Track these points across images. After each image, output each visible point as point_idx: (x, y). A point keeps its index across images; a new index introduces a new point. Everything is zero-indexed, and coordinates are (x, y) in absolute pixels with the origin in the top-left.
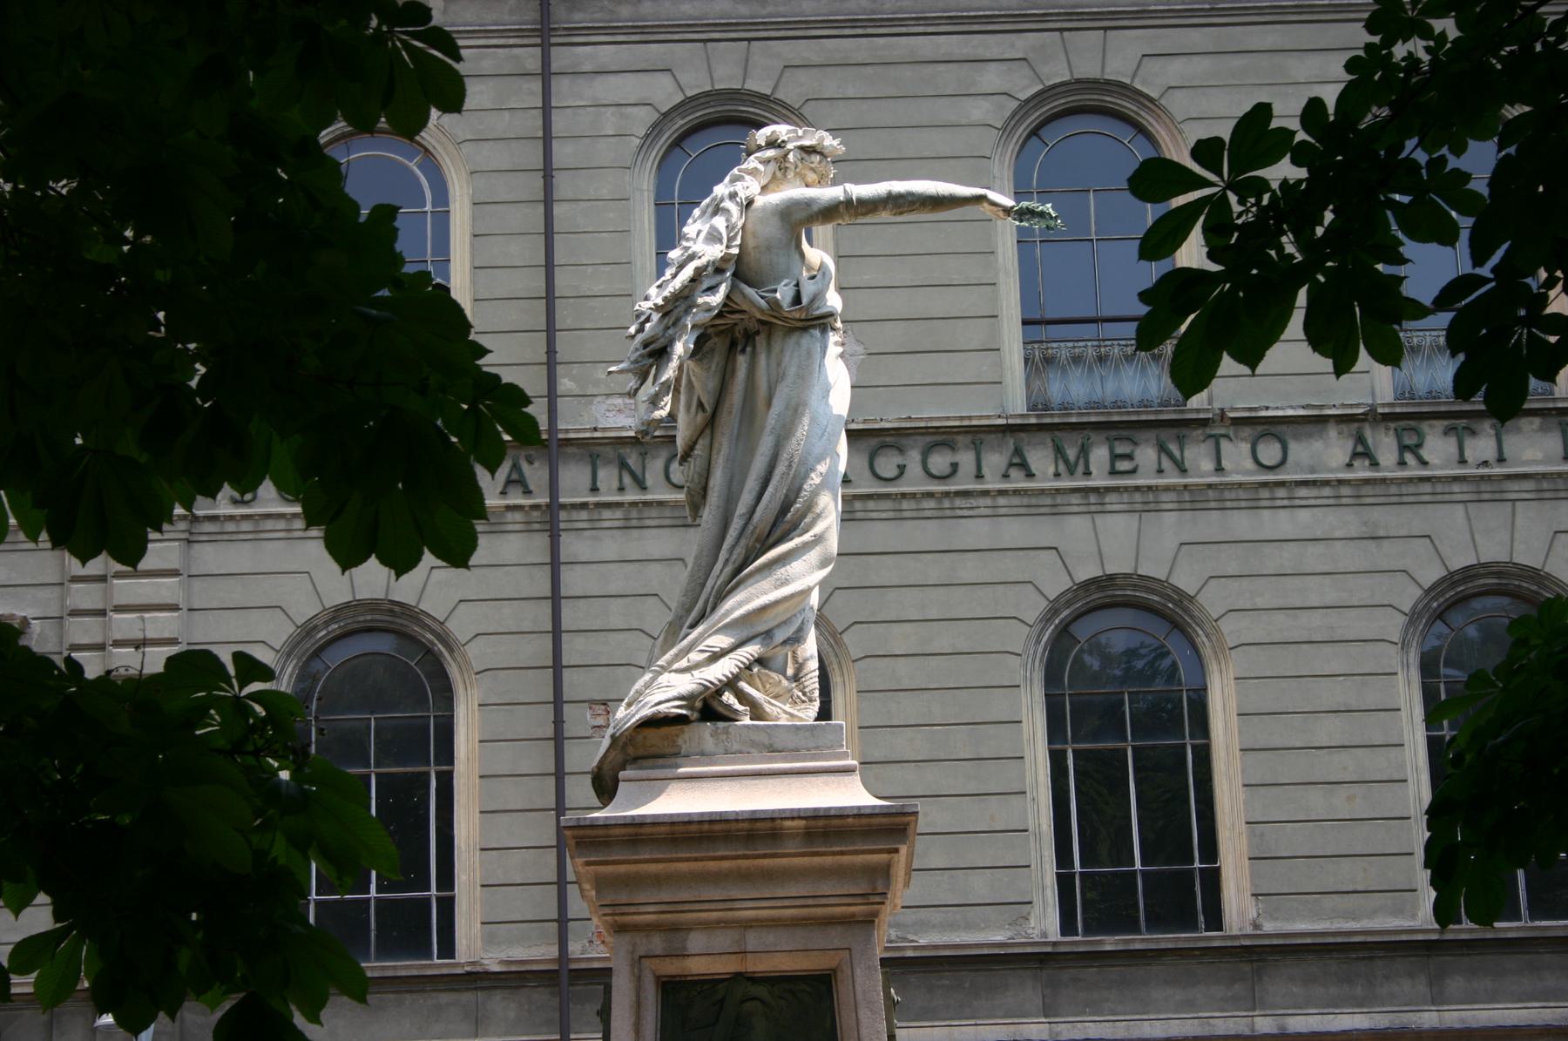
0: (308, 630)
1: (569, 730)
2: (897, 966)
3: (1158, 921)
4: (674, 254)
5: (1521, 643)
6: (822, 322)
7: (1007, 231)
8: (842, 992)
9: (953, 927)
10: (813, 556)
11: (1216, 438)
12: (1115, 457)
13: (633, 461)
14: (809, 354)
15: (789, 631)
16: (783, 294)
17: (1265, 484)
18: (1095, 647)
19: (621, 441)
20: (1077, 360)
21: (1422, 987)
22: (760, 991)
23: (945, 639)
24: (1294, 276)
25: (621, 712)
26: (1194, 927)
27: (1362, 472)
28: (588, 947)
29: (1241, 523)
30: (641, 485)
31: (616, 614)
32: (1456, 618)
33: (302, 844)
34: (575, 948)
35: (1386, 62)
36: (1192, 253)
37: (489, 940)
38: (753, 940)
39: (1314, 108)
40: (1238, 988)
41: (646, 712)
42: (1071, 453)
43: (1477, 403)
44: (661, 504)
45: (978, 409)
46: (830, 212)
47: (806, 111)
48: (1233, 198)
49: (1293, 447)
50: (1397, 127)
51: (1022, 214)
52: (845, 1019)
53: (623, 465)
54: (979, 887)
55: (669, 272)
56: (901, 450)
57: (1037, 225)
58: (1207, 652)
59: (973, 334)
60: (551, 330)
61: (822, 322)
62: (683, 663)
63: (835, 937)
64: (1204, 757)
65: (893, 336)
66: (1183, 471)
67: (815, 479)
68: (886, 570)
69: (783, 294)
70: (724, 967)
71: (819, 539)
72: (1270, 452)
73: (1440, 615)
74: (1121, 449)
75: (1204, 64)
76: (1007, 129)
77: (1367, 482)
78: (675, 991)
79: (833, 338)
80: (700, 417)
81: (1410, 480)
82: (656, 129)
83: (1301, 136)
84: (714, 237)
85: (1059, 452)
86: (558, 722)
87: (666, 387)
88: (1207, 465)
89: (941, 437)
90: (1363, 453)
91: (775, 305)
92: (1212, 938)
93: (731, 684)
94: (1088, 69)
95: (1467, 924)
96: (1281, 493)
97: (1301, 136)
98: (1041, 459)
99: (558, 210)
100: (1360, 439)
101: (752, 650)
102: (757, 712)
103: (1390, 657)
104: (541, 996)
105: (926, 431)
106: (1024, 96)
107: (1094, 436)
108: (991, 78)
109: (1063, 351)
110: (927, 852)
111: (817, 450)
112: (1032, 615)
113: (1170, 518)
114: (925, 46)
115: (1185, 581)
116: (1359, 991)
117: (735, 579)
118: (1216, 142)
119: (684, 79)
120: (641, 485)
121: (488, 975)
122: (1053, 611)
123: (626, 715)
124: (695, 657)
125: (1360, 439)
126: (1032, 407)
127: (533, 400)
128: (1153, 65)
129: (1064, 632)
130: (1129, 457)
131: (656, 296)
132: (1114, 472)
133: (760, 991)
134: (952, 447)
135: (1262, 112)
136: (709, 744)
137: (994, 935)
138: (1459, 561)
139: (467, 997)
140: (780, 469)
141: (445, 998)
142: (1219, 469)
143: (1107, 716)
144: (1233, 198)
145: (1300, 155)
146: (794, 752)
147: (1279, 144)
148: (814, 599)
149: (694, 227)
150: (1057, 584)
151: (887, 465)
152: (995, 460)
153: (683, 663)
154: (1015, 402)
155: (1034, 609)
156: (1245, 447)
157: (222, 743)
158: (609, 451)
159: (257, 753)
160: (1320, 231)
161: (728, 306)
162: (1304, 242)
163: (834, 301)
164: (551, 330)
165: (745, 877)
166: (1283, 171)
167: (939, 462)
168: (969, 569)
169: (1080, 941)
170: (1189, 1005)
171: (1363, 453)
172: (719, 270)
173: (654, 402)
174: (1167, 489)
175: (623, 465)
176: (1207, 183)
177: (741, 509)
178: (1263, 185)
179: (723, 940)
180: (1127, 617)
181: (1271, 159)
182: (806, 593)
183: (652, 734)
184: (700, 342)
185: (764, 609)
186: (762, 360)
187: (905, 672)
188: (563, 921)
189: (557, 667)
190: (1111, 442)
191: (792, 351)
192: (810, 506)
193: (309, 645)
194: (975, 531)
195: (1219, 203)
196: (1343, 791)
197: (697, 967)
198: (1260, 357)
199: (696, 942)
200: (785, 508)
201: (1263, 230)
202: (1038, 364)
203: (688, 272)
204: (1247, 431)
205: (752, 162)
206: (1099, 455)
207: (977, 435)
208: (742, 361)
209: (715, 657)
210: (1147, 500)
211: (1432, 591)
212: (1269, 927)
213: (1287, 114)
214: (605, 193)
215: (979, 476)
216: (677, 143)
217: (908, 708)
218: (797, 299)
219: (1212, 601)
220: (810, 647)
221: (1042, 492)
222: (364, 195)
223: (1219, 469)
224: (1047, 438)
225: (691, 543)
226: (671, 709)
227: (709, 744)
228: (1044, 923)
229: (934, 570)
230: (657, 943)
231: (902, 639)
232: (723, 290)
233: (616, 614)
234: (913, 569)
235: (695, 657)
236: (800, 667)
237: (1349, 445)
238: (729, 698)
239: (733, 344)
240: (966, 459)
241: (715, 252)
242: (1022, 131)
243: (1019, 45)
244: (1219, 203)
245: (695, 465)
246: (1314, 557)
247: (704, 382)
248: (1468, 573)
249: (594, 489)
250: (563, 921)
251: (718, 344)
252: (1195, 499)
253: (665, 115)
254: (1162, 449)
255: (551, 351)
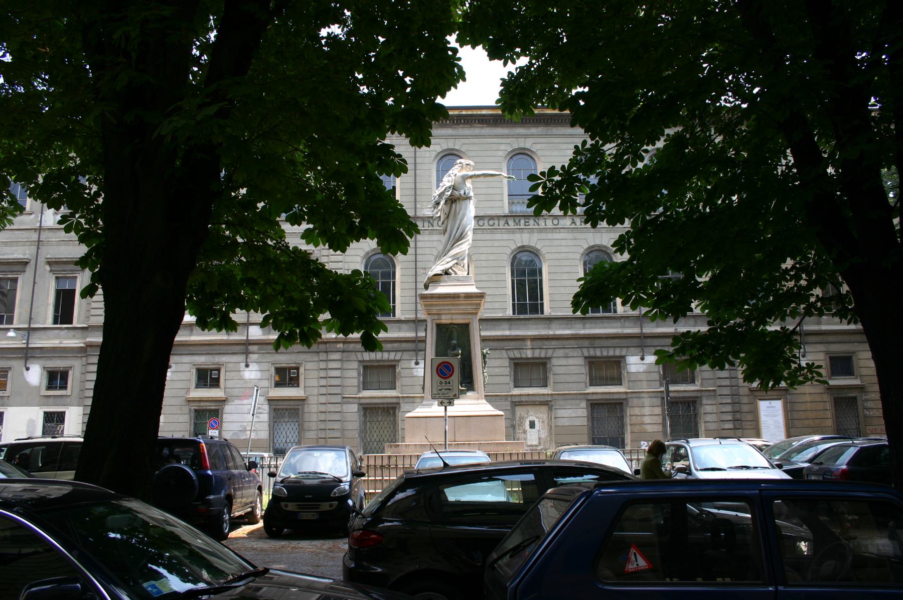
0: (368, 253)
1: (418, 273)
2: (482, 320)
3: (531, 312)
4: (441, 184)
5: (595, 268)
6: (469, 198)
7: (505, 181)
8: (471, 327)
9: (491, 313)
10: (467, 243)
11: (545, 219)
12: (526, 222)
13: (431, 221)
14: (467, 204)
15: (462, 258)
16: (462, 192)
17: (554, 228)
18: (520, 260)
19: (429, 217)
20: (518, 203)
21: (581, 326)
22: (456, 326)
23: (491, 257)
24: (557, 198)
25: (430, 273)
26: (538, 314)
27: (573, 226)
28: (422, 316)
29: (550, 236)
30: (433, 226)
31: (427, 251)
32: (591, 255)
33: (374, 305)
34: (419, 316)
35: (577, 159)
36: (540, 191)
37: (402, 314)
38: (454, 317)
39: (563, 167)
40: (546, 326)
41: (435, 273)
42: (517, 221)
43: (589, 225)
44: (436, 230)
45: (500, 213)
46: (471, 177)
47: (467, 153)
48: (547, 182)
49: (560, 221)
50: (578, 171)
51: (509, 178)
52: (471, 332)
53: (429, 222)
54: (497, 305)
55: (440, 188)
56: (484, 220)
57: (511, 180)
58: (542, 260)
59: (498, 197)
60: (415, 195)
61: (469, 198)
62: (442, 264)
63: (470, 316)
64: (541, 281)
65: (482, 197)
66: (539, 225)
67: (467, 229)
68: (480, 244)
69: (462, 192)
70: (449, 322)
71: (468, 240)
72: (556, 222)
73: (587, 254)
74: (527, 220)
75: (544, 145)
76: (506, 157)
77: (574, 228)
78: (439, 326)
79: (471, 201)
80: (446, 216)
81: (582, 228)
82: (437, 156)
83: (561, 172)
84: (449, 181)
85: (515, 221)
86: (416, 272)
87: (439, 210)
88: (543, 224)
89: (492, 218)
90: (573, 222)
91: (460, 195)
92: (542, 316)
93: (451, 268)
94: (522, 146)
95: (590, 314)
96: (557, 230)
97: (561, 172)
98: (511, 222)
99: (417, 171)
100: (573, 220)
101: (455, 261)
102: (456, 273)
103: (578, 263)
104: (412, 325)
105: (489, 216)
106: (509, 150)
107: (522, 218)
108: (503, 147)
109: (516, 201)
110: (487, 299)
111: (468, 223)
112: (509, 253)
113: (536, 234)
114: (490, 140)
115: (538, 247)
116: (569, 326)
117: (452, 247)
118: (544, 172)
119: (442, 146)
120: (433, 226)
121: (402, 320)
122: (513, 252)
123: (431, 273)
124: (444, 262)
125: (573, 220)
126: (510, 212)
127: (420, 224)
128: (534, 145)
129: (514, 258)
130: (528, 222)
131: (438, 192)
132: (525, 225)
133: (456, 326)
134: (493, 219)
135: (553, 167)
136: (446, 279)
137: (500, 315)
138: (592, 244)
139: (398, 325)
140: (461, 226)
141: (393, 325)
142: (546, 225)
143: (523, 273)
144: (547, 182)
145: (560, 175)
146: (463, 281)
147: (557, 173)
148: (467, 252)
149: (445, 179)
150: (514, 247)
151: (481, 223)
152: (502, 222)
153: (442, 264)
154: (506, 211)
155: (509, 251)
156: (551, 221)
157: (361, 287)
158: (426, 219)
159: (367, 289)
160: (563, 189)
161: (451, 195)
162: (560, 190)
163: (472, 194)
164: (415, 195)
165: (453, 305)
166: (557, 178)
167: (491, 222)
168: (496, 243)
169: (516, 316)
170: (537, 329)
171: (573, 222)
172: (450, 188)
173: (437, 213)
174: (536, 229)
175: (429, 222)
176: (542, 179)
177: (453, 234)
178: (553, 180)
179: (449, 317)
180: (527, 253)
181: (555, 176)
182: (465, 251)
183: (435, 277)
184: (446, 201)
185: (457, 254)
186: (458, 205)
187: (484, 264)
188: (416, 310)
189: (416, 261)
190: (525, 219)
191: (463, 203)
192: (466, 234)
193: (368, 256)
194: (498, 236)
195: (545, 183)
196: (568, 288)
197: (443, 321)
198: (551, 211)
199: (443, 317)
200: (462, 234)
201: (551, 189)
202: (511, 203)
203: (444, 188)
204: (551, 218)
205: (456, 167)
206: (522, 222)
207: (499, 217)
208: (454, 205)
209: (448, 263)
210: (532, 231)
211: (586, 250)
212: (552, 314)
213: (558, 168)
214: (426, 168)
215: (499, 225)
216: (441, 158)
217: (484, 271)
218: (465, 194)
219: (543, 251)
220: (466, 261)
221: (511, 229)
222: (389, 187)
223: (546, 225)
224: (512, 218)
225: (444, 239)
226: (439, 272)
227: (446, 279)
228: (509, 313)
229: (489, 243)
230: (436, 317)
231: (483, 257)
232: (450, 191)
233: (427, 251)
234: (485, 243)
235: (444, 262)
236: (464, 265)
237: (571, 221)
238: (450, 270)
239: (452, 202)
240: (496, 222)
241: (449, 184)
242: (509, 158)
243: (508, 141)
244: (545, 183)
245: (444, 225)
246: (564, 243)
247: (447, 209)
248: (593, 246)
249: (424, 227)
250: (416, 310)
251: (449, 202)
252: (541, 231)
253: (439, 153)
254: (535, 221)
255: (415, 199)
